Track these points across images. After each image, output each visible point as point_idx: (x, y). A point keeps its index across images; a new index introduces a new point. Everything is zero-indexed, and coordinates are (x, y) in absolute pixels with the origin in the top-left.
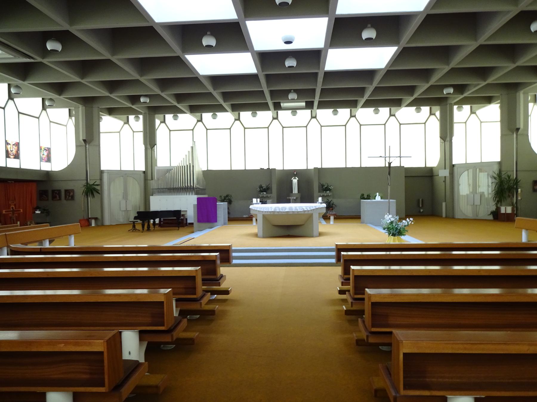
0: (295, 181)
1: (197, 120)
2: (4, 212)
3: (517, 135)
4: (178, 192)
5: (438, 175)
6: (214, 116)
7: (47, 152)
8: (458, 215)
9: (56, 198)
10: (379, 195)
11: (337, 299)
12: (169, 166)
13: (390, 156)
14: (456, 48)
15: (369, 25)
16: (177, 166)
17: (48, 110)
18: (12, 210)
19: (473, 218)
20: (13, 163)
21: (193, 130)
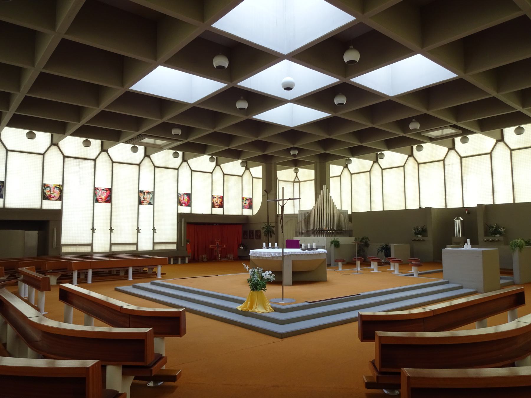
0: (458, 222)
1: (449, 149)
2: (211, 246)
6: (519, 131)
7: (249, 201)
12: (340, 209)
16: (312, 209)
17: (251, 169)
20: (218, 211)
21: (404, 166)
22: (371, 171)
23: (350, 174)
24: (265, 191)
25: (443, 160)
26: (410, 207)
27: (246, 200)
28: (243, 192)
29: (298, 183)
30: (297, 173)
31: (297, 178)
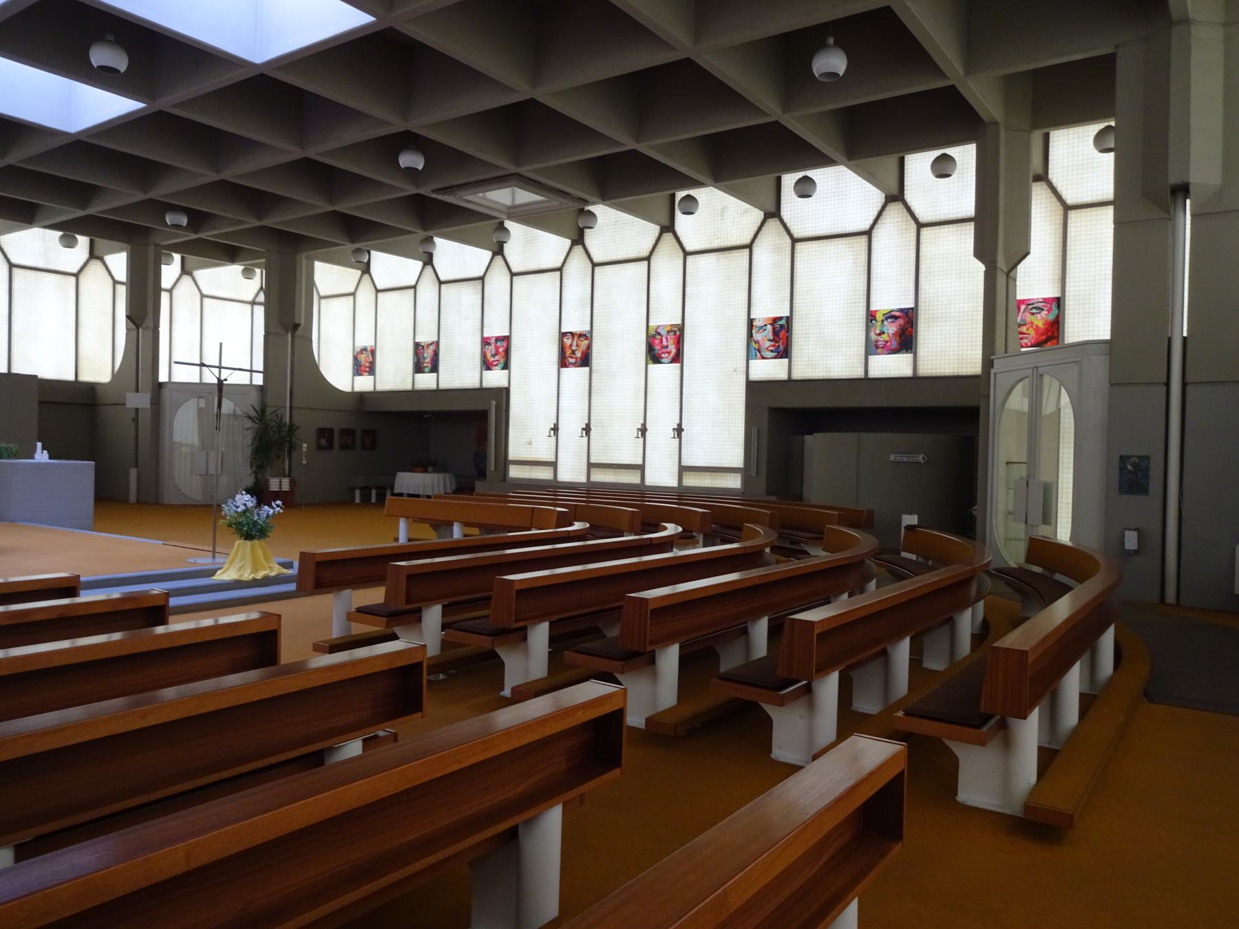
1: (765, 214)
3: (293, 337)
5: (125, 404)
7: (901, 321)
8: (169, 497)
10: (44, 448)
13: (223, 365)
14: (244, 146)
15: (110, 37)
19: (204, 503)
23: (509, 274)
27: (887, 319)
28: (509, 302)
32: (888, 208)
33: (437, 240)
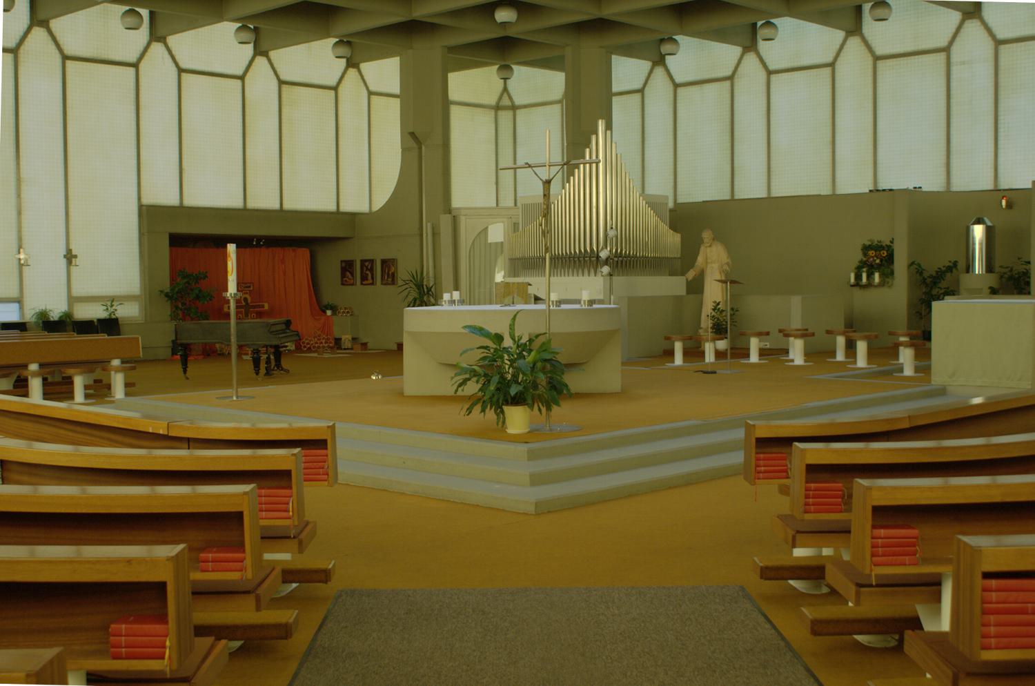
4: (563, 267)
9: (367, 280)
11: (806, 475)
17: (364, 66)
18: (244, 304)
21: (832, 65)
22: (736, 76)
23: (672, 85)
24: (412, 134)
25: (947, 50)
26: (845, 187)
29: (510, 113)
30: (505, 79)
31: (505, 95)
32: (848, 42)
33: (515, 67)
